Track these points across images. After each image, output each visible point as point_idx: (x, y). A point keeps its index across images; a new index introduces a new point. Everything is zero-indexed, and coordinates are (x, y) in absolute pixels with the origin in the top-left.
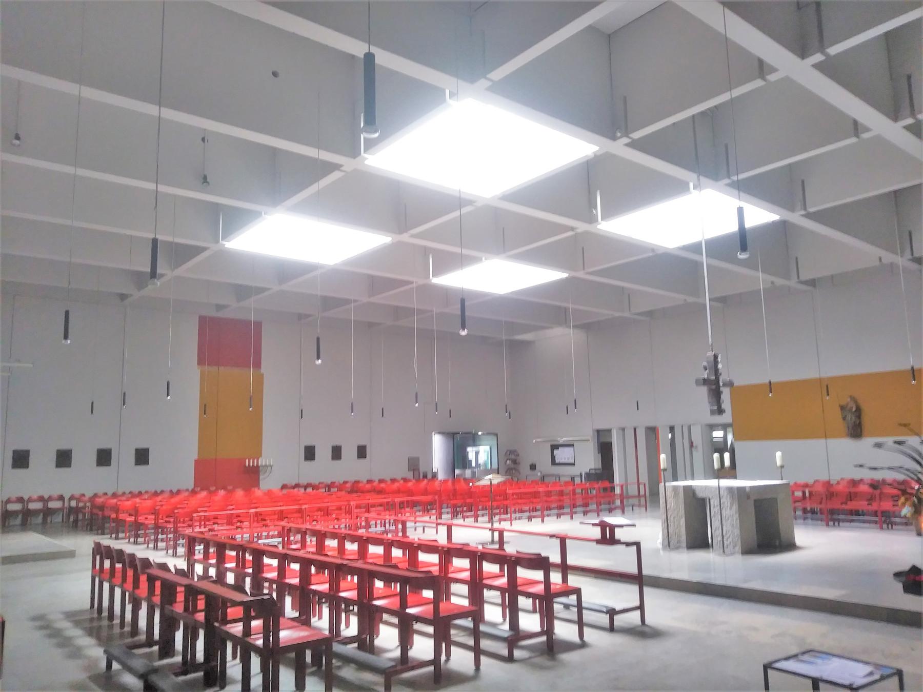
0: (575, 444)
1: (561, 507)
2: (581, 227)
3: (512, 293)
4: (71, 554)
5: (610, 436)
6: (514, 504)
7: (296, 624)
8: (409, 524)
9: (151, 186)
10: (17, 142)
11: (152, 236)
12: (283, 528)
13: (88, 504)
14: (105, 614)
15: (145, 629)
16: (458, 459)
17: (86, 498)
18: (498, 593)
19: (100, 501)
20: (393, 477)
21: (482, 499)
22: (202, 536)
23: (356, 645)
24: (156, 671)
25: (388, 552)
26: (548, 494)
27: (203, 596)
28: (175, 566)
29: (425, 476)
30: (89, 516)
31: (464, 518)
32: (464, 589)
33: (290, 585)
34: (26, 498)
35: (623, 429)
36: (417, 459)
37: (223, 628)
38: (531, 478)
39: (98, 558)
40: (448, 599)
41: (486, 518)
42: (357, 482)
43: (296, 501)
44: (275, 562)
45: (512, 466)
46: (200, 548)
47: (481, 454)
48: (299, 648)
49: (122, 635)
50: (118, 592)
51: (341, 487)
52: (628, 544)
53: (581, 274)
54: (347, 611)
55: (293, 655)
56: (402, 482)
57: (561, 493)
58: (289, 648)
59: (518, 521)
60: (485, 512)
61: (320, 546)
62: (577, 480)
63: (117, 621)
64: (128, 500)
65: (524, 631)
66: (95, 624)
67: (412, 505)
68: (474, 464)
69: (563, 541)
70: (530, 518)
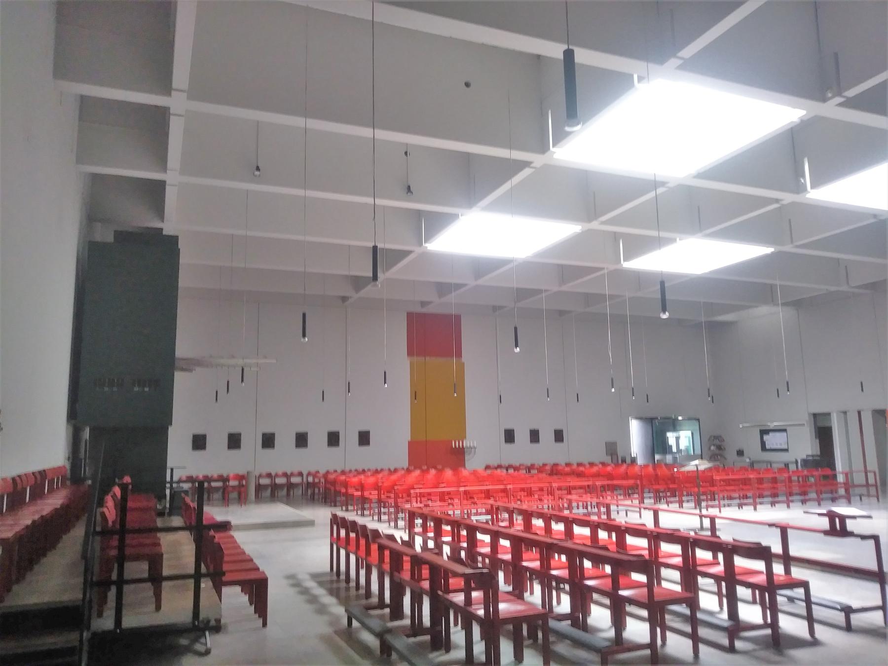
0: (788, 429)
1: (775, 495)
2: (788, 198)
3: (711, 272)
4: (310, 523)
5: (830, 420)
6: (722, 491)
7: (512, 598)
8: (613, 508)
9: (370, 200)
10: (257, 173)
11: (371, 244)
12: (492, 506)
13: (323, 480)
14: (343, 577)
15: (377, 593)
16: (657, 442)
17: (321, 475)
18: (712, 581)
19: (332, 477)
20: (591, 460)
21: (687, 485)
22: (420, 511)
23: (569, 622)
24: (390, 631)
25: (594, 535)
26: (760, 481)
27: (427, 566)
28: (401, 538)
29: (624, 461)
30: (324, 490)
31: (668, 503)
32: (676, 575)
33: (503, 561)
34: (273, 474)
35: (845, 413)
36: (556, 441)
37: (446, 596)
38: (739, 465)
39: (335, 528)
40: (659, 583)
41: (692, 505)
42: (556, 465)
43: (500, 481)
44: (487, 538)
45: (717, 452)
46: (419, 521)
47: (682, 439)
48: (516, 621)
49: (358, 597)
50: (353, 558)
51: (541, 469)
52: (863, 537)
53: (788, 248)
54: (558, 589)
55: (511, 627)
56: (600, 466)
57: (774, 480)
58: (507, 621)
59: (727, 509)
60: (690, 498)
61: (528, 526)
62: (792, 467)
63: (353, 584)
64: (354, 476)
65: (743, 622)
66: (335, 585)
67: (613, 488)
68: (674, 449)
69: (784, 531)
70: (740, 506)
